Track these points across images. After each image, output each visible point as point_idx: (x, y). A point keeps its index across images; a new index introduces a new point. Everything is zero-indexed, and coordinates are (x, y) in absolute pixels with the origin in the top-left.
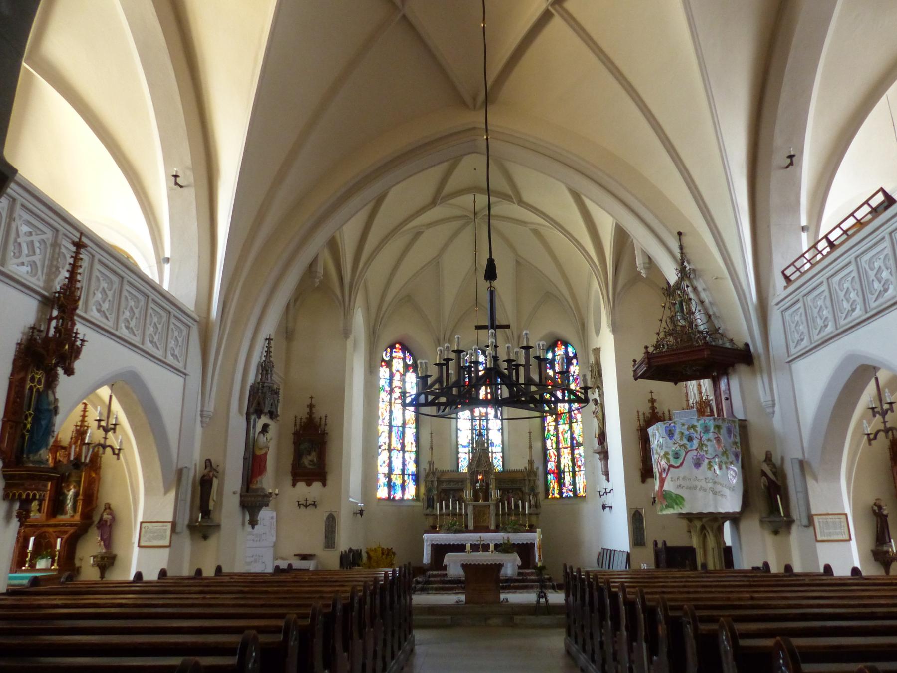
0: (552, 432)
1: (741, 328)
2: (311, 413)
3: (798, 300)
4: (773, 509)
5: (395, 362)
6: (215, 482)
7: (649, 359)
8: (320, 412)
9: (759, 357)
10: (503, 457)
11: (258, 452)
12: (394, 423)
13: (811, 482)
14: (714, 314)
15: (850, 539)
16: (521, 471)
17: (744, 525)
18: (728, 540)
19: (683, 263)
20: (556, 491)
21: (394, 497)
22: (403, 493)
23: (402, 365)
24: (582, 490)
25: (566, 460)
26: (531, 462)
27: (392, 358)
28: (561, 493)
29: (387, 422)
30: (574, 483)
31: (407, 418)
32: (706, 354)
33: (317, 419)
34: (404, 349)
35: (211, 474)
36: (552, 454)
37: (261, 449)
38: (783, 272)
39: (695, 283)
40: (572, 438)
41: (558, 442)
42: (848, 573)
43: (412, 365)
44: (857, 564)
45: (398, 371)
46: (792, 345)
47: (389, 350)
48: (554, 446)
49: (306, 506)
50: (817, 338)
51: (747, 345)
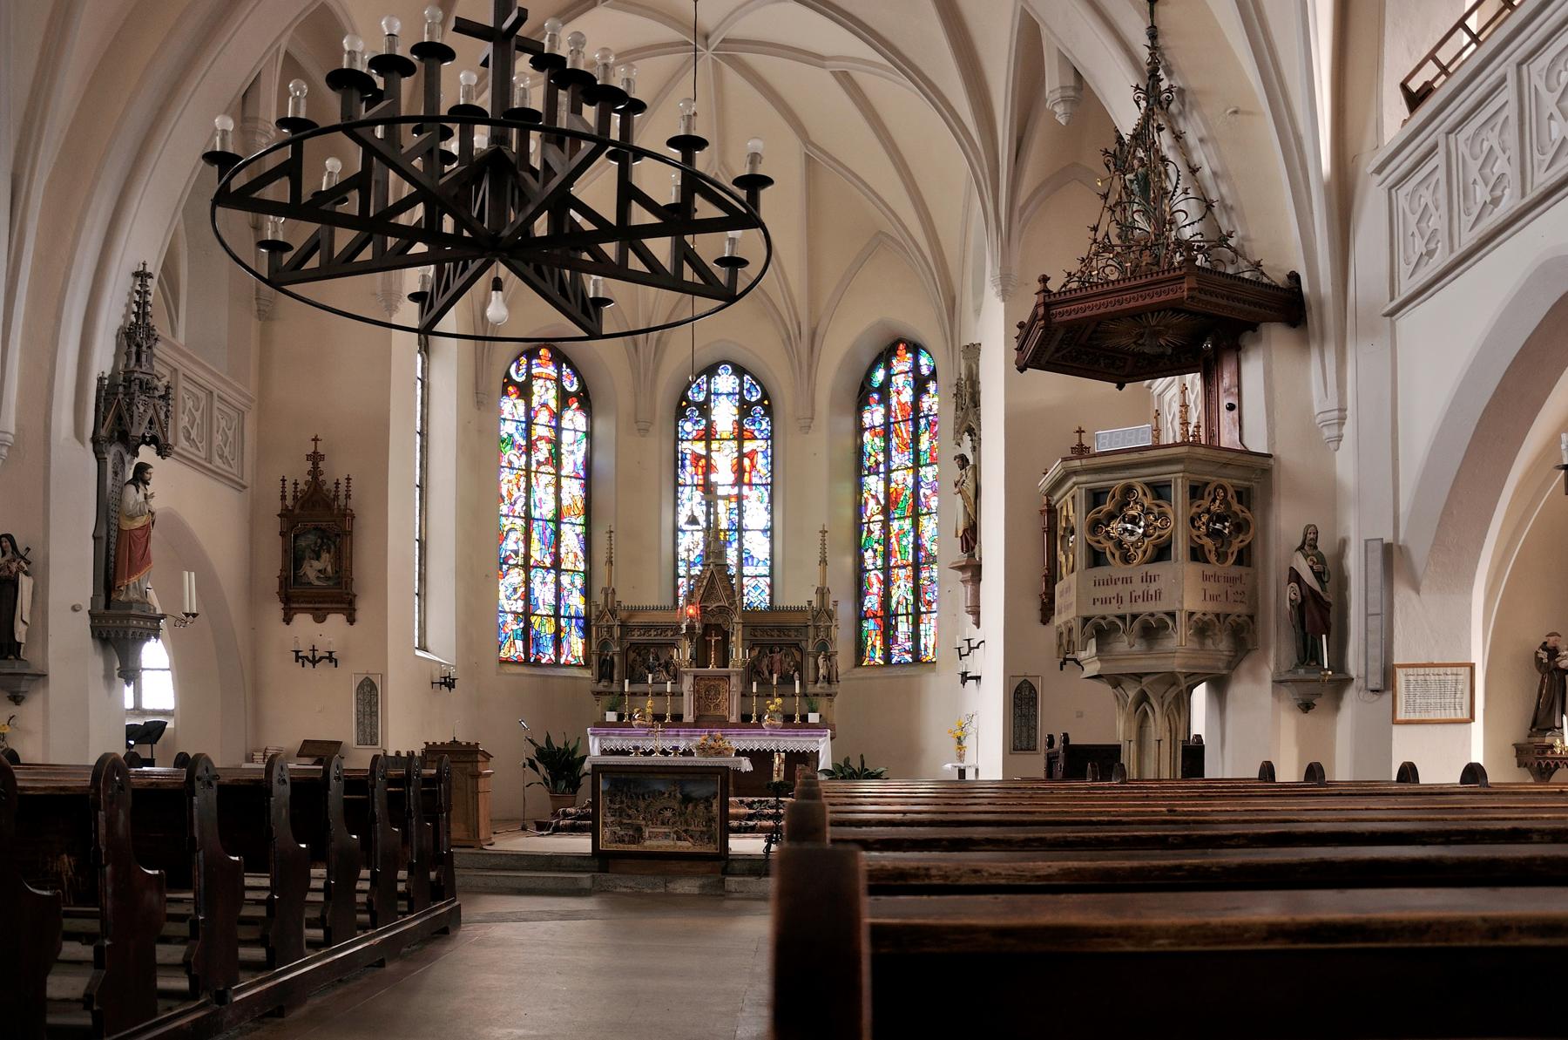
0: (877, 534)
1: (1282, 240)
2: (315, 472)
3: (1433, 149)
4: (1308, 654)
5: (537, 386)
6: (26, 584)
7: (1047, 306)
8: (334, 471)
9: (1321, 304)
10: (771, 586)
11: (127, 525)
12: (536, 514)
13: (1402, 593)
14: (1222, 200)
15: (1472, 717)
16: (800, 610)
17: (1239, 690)
18: (1199, 724)
19: (1154, 77)
20: (879, 653)
21: (537, 661)
22: (558, 653)
23: (553, 393)
24: (930, 651)
25: (901, 591)
26: (822, 592)
27: (530, 377)
28: (887, 656)
29: (519, 508)
30: (915, 636)
31: (566, 500)
32: (1184, 290)
33: (330, 485)
34: (559, 359)
35: (14, 567)
36: (874, 580)
37: (132, 518)
38: (1404, 86)
39: (1182, 125)
40: (917, 547)
41: (887, 555)
42: (1453, 777)
43: (576, 394)
44: (1477, 757)
45: (544, 405)
46: (1404, 270)
47: (524, 360)
48: (879, 562)
49: (314, 662)
50: (1467, 239)
51: (1294, 277)
